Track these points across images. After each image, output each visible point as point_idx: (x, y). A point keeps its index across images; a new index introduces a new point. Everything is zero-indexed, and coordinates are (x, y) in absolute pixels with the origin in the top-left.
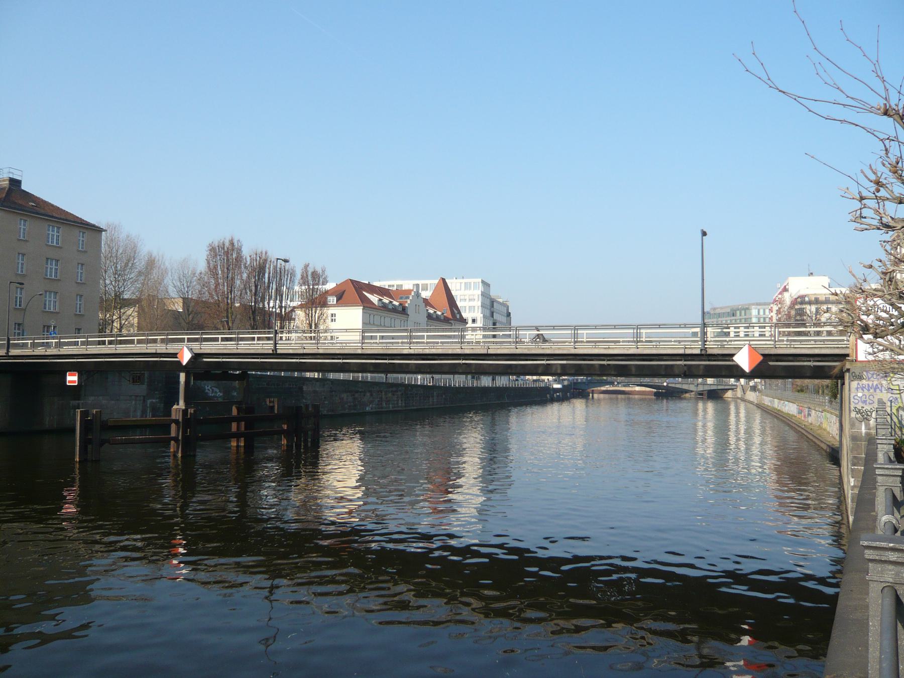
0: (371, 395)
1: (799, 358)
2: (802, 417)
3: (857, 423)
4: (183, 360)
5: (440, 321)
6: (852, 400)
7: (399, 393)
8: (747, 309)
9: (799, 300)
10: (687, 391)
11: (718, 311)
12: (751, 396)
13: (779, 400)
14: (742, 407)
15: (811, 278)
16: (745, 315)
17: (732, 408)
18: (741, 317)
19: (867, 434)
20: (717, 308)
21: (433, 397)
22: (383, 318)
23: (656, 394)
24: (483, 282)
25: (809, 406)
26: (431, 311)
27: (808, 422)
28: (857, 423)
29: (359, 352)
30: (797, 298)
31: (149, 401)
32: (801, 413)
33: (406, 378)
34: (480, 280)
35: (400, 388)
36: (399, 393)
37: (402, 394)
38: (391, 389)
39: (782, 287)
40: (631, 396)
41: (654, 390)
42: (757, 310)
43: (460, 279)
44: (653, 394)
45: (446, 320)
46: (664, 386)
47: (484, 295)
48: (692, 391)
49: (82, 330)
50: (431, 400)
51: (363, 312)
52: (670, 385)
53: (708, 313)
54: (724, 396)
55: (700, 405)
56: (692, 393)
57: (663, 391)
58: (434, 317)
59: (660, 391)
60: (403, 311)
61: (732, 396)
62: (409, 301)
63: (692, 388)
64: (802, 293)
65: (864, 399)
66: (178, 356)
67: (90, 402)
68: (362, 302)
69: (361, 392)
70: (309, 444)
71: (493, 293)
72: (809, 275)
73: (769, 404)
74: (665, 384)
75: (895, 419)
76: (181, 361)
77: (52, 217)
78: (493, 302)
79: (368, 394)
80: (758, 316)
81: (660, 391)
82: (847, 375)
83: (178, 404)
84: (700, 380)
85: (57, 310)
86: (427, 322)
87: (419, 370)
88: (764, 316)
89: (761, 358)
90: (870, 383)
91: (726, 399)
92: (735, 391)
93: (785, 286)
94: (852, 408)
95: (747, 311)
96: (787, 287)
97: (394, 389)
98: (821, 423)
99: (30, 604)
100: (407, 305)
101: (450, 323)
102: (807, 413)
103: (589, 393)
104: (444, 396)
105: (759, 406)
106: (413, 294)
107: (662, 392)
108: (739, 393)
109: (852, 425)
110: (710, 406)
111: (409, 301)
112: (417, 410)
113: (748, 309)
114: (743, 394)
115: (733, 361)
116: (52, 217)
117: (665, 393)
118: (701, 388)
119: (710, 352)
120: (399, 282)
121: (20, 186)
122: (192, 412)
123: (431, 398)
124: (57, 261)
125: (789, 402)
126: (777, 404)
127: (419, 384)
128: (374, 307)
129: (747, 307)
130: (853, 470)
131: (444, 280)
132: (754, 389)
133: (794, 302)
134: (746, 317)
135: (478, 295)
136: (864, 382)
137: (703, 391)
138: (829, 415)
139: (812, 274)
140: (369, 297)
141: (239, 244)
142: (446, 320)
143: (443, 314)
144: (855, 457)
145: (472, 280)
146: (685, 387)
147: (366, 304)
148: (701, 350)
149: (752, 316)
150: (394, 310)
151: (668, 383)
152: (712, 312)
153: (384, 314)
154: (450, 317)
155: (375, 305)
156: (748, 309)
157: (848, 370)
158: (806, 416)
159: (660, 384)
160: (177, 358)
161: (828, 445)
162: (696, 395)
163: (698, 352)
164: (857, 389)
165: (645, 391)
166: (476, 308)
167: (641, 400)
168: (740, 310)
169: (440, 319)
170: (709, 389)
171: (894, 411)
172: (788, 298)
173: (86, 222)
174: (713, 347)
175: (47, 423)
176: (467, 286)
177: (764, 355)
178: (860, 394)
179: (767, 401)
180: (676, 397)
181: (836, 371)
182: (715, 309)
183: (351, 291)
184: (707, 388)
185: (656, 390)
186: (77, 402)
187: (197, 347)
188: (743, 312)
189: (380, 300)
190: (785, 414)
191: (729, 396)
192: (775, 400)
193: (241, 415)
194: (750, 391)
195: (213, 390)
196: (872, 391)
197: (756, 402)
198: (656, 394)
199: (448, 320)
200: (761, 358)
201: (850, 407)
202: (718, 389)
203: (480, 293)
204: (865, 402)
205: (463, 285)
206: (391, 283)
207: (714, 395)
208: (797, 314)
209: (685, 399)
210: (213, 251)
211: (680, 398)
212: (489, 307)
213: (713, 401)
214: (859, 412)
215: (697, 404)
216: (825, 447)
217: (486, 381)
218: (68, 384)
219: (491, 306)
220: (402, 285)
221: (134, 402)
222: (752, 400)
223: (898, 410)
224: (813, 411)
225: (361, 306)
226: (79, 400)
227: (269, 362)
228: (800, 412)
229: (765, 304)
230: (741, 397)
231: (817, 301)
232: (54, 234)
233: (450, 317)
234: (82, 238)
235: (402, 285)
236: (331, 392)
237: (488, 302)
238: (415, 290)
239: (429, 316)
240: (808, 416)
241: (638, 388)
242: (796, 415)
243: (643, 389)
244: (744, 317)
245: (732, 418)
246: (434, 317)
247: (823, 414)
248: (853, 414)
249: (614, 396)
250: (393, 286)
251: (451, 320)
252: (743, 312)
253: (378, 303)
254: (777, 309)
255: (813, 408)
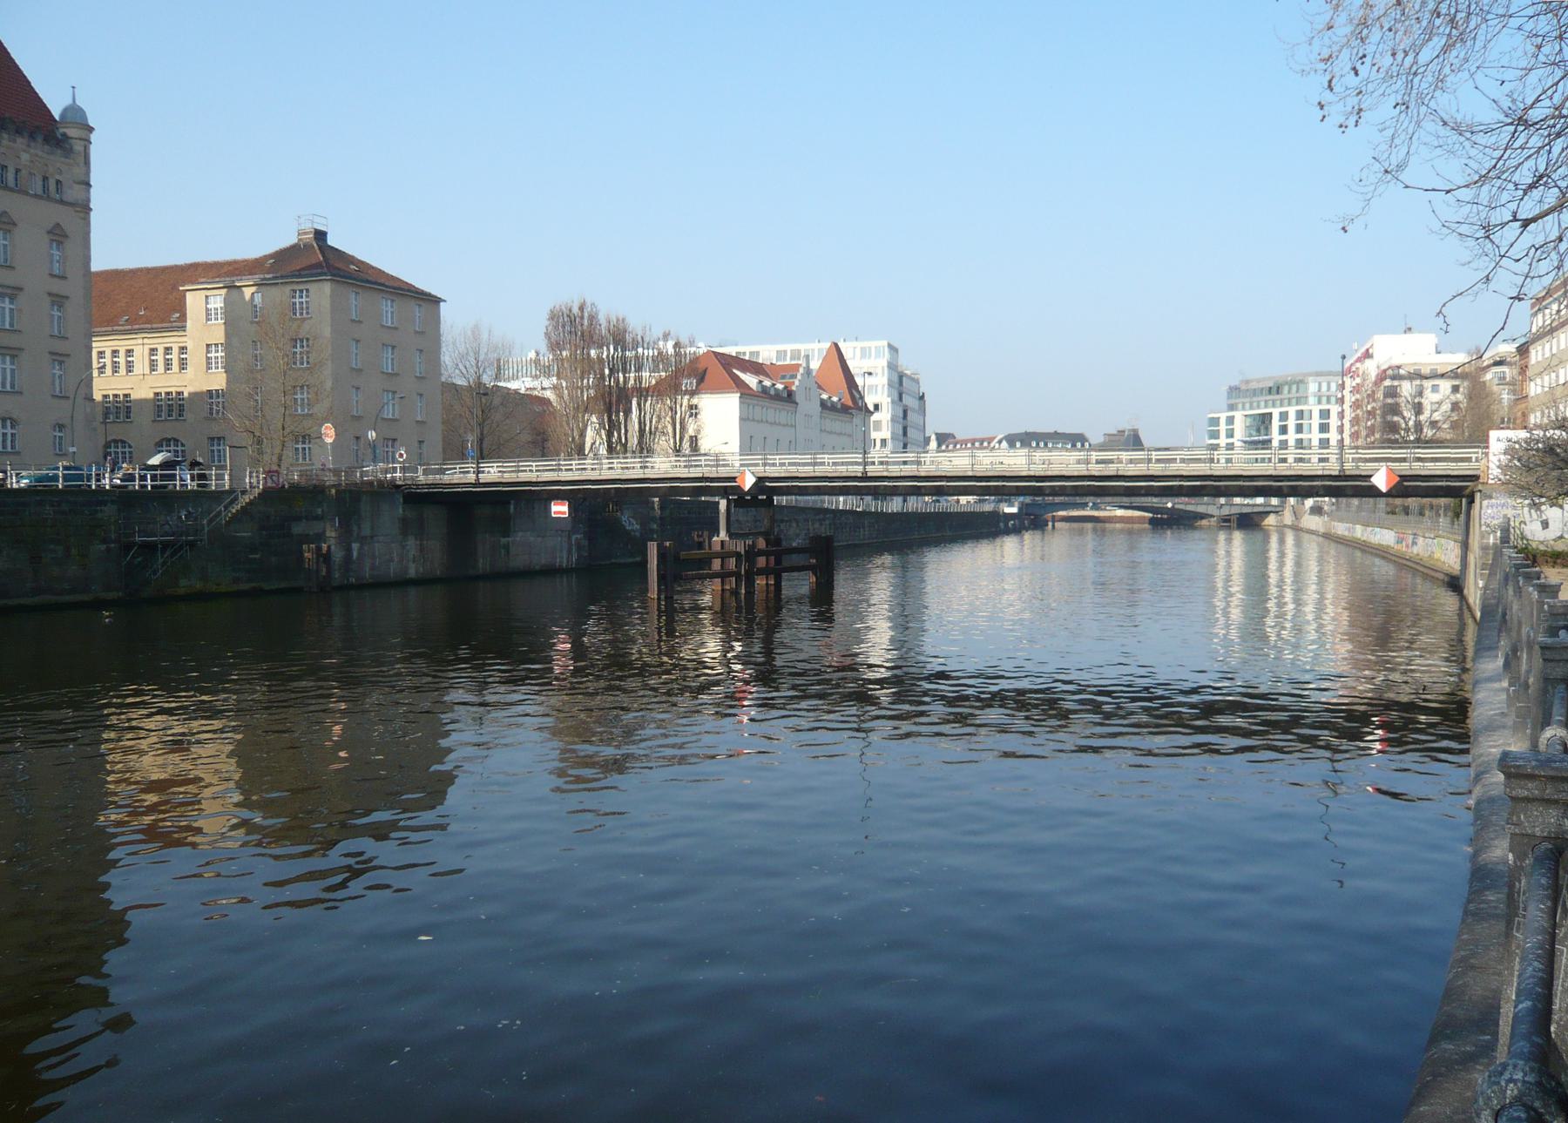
0: (798, 526)
1: (1432, 479)
2: (1403, 548)
3: (1486, 535)
4: (744, 486)
5: (781, 401)
6: (1483, 516)
7: (827, 522)
8: (1300, 382)
9: (1390, 372)
10: (1203, 516)
11: (1254, 385)
12: (1312, 522)
13: (1363, 528)
14: (1290, 539)
15: (1408, 336)
16: (1297, 391)
17: (1274, 539)
18: (1290, 396)
19: (1494, 543)
20: (1252, 381)
21: (864, 528)
22: (751, 407)
23: (1152, 521)
24: (890, 346)
25: (1415, 531)
26: (825, 396)
27: (1412, 553)
28: (1486, 535)
29: (970, 474)
30: (1388, 369)
31: (574, 537)
32: (1401, 543)
33: (828, 502)
34: (885, 343)
35: (828, 516)
36: (827, 522)
37: (830, 524)
38: (817, 517)
39: (1363, 350)
40: (1107, 525)
41: (1146, 514)
42: (1317, 384)
43: (851, 341)
44: (1147, 521)
45: (845, 409)
46: (1167, 508)
47: (892, 366)
48: (1212, 516)
49: (399, 440)
50: (862, 533)
51: (741, 403)
52: (1176, 506)
53: (1236, 389)
54: (1263, 524)
55: (1222, 536)
56: (1212, 519)
57: (1165, 516)
58: (772, 392)
59: (1159, 516)
60: (788, 397)
61: (1275, 524)
62: (797, 383)
63: (1212, 510)
64: (1396, 362)
65: (1492, 515)
66: (737, 480)
67: (518, 539)
68: (737, 386)
69: (787, 521)
70: (189, 658)
71: (907, 365)
72: (1405, 332)
73: (1346, 533)
74: (1169, 505)
75: (1518, 532)
76: (742, 486)
77: (383, 285)
78: (901, 377)
79: (794, 525)
80: (1319, 394)
81: (1159, 516)
82: (1478, 496)
83: (718, 536)
84: (1222, 500)
85: (397, 416)
86: (821, 412)
87: (845, 491)
88: (1328, 393)
89: (1398, 479)
90: (1499, 502)
91: (1267, 527)
92: (1280, 515)
93: (1367, 350)
94: (1483, 523)
95: (1301, 385)
96: (1370, 351)
97: (821, 516)
98: (1433, 553)
99: (422, 795)
100: (794, 388)
101: (851, 414)
102: (1410, 542)
103: (1047, 521)
104: (876, 527)
105: (1328, 536)
106: (801, 370)
107: (1161, 518)
108: (1288, 518)
109: (1482, 537)
110: (1238, 536)
111: (797, 383)
112: (849, 546)
113: (1301, 381)
114: (1294, 519)
115: (1370, 482)
116: (375, 283)
117: (1168, 519)
118: (1226, 511)
119: (1348, 473)
120: (754, 348)
121: (326, 241)
122: (751, 543)
123: (862, 530)
124: (393, 347)
125: (1381, 528)
126: (1359, 532)
127: (841, 508)
128: (750, 392)
129: (1301, 378)
130: (1482, 574)
131: (836, 345)
132: (1316, 510)
133: (1382, 376)
134: (1298, 395)
135: (883, 367)
136: (1493, 501)
137: (1230, 515)
138: (1443, 541)
139: (1410, 329)
140: (743, 379)
141: (594, 310)
142: (845, 409)
143: (840, 400)
144: (1484, 564)
145: (873, 344)
146: (1201, 509)
147: (741, 386)
148: (1340, 471)
149: (1309, 395)
150: (777, 397)
151: (1174, 504)
152: (1244, 387)
153: (767, 403)
154: (850, 403)
155: (751, 389)
156: (1301, 381)
157: (1480, 491)
158: (1410, 545)
159: (1161, 505)
160: (736, 482)
161: (1445, 574)
162: (1219, 522)
163: (1337, 473)
164: (1488, 507)
165: (1132, 517)
166: (880, 388)
167: (1122, 531)
168: (1290, 384)
169: (783, 397)
170: (1239, 512)
171: (1517, 524)
172: (1371, 368)
173: (423, 291)
174: (1350, 468)
175: (480, 565)
176: (865, 353)
177: (1400, 476)
178: (1489, 511)
179: (1341, 529)
180: (1185, 525)
181: (1467, 491)
182: (1247, 382)
183: (716, 370)
184: (1235, 510)
185: (1151, 515)
186: (507, 539)
187: (761, 471)
188: (1294, 387)
189: (761, 382)
190: (1375, 545)
191: (1271, 523)
192: (1358, 526)
193: (770, 548)
194: (1309, 514)
195: (630, 522)
196: (1500, 508)
197: (1322, 530)
198: (1152, 521)
199: (847, 410)
200: (1398, 479)
201: (1480, 523)
202: (1253, 513)
203: (885, 364)
204: (1493, 518)
205: (858, 352)
206: (740, 349)
207: (1248, 522)
208: (1386, 396)
209: (1201, 528)
210: (553, 316)
211: (1192, 527)
212: (897, 386)
213: (1243, 532)
214: (1488, 526)
215: (1217, 537)
216: (1441, 576)
217: (895, 505)
218: (553, 515)
219: (900, 383)
220: (758, 353)
221: (559, 539)
222: (1313, 527)
223: (1520, 524)
224: (1421, 539)
225: (737, 392)
226: (508, 537)
227: (955, 486)
228: (1400, 541)
229: (1329, 374)
230: (1293, 525)
231: (1417, 375)
232: (388, 310)
233: (850, 403)
234: (417, 311)
235: (758, 353)
236: (756, 521)
237: (896, 379)
238: (804, 365)
239: (823, 404)
240: (1413, 545)
241: (1120, 512)
242: (1392, 545)
243: (1130, 513)
244: (1295, 395)
245: (1273, 554)
246: (829, 404)
247: (1435, 541)
248: (1483, 528)
249: (1075, 525)
250: (744, 353)
251: (850, 408)
252: (1294, 387)
253: (757, 387)
254: (1354, 384)
255: (1421, 534)
